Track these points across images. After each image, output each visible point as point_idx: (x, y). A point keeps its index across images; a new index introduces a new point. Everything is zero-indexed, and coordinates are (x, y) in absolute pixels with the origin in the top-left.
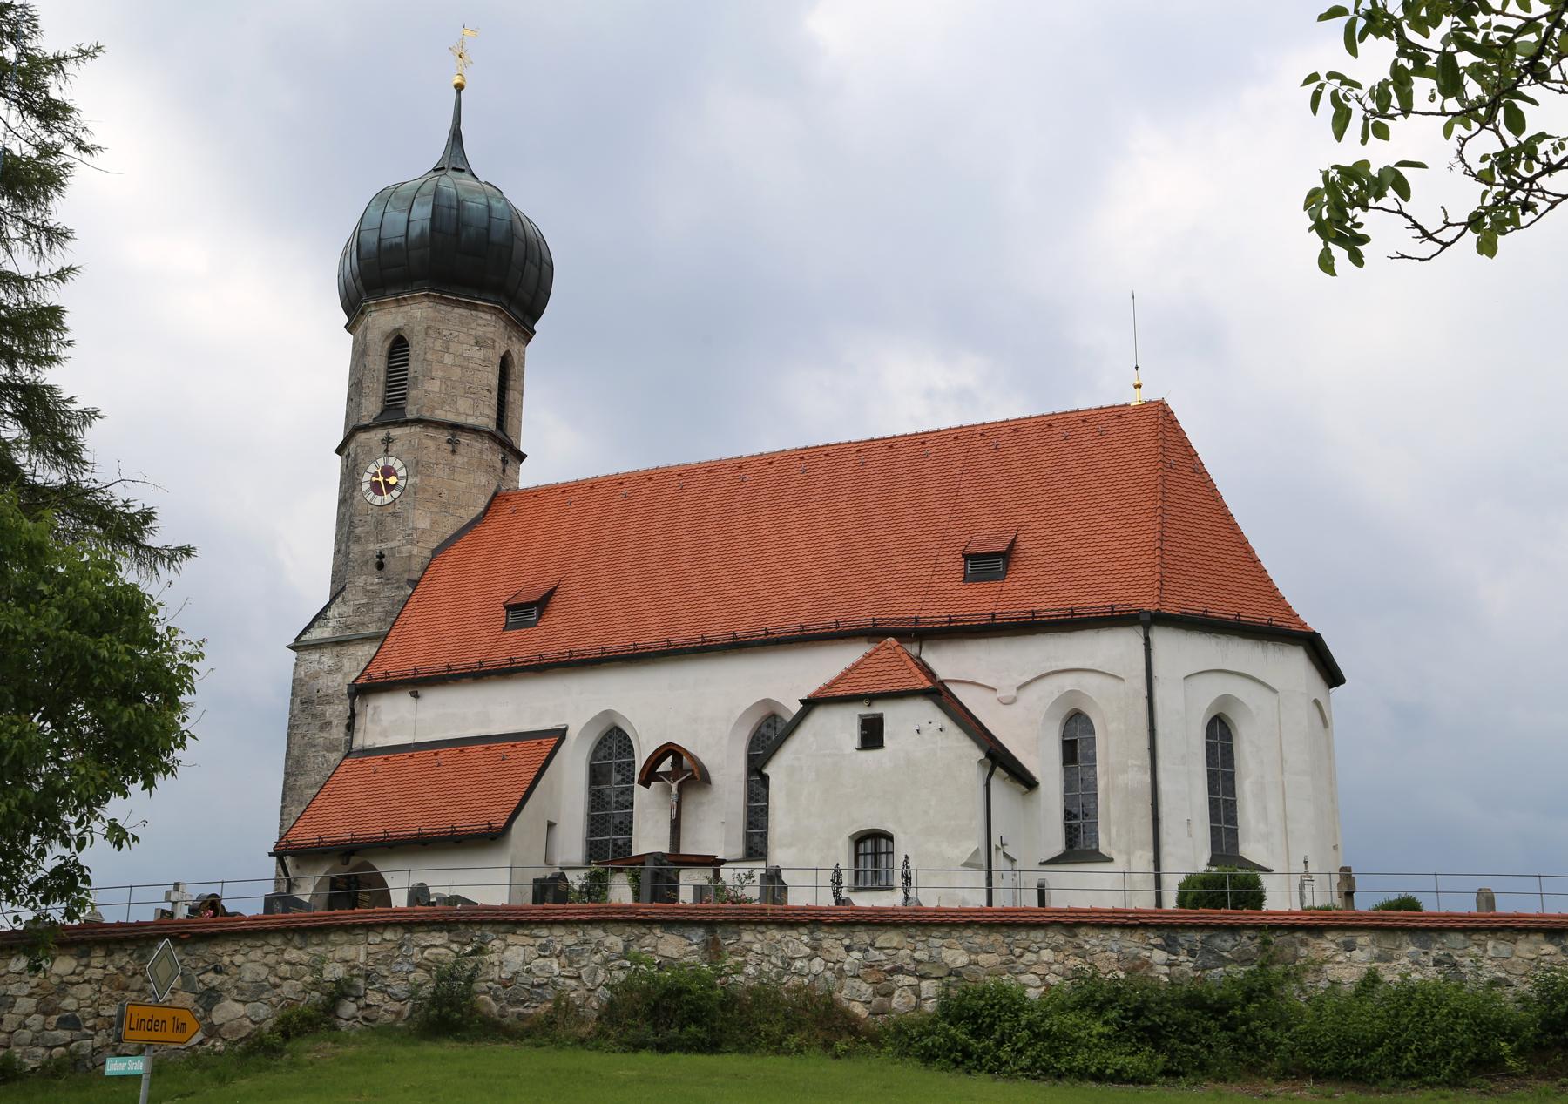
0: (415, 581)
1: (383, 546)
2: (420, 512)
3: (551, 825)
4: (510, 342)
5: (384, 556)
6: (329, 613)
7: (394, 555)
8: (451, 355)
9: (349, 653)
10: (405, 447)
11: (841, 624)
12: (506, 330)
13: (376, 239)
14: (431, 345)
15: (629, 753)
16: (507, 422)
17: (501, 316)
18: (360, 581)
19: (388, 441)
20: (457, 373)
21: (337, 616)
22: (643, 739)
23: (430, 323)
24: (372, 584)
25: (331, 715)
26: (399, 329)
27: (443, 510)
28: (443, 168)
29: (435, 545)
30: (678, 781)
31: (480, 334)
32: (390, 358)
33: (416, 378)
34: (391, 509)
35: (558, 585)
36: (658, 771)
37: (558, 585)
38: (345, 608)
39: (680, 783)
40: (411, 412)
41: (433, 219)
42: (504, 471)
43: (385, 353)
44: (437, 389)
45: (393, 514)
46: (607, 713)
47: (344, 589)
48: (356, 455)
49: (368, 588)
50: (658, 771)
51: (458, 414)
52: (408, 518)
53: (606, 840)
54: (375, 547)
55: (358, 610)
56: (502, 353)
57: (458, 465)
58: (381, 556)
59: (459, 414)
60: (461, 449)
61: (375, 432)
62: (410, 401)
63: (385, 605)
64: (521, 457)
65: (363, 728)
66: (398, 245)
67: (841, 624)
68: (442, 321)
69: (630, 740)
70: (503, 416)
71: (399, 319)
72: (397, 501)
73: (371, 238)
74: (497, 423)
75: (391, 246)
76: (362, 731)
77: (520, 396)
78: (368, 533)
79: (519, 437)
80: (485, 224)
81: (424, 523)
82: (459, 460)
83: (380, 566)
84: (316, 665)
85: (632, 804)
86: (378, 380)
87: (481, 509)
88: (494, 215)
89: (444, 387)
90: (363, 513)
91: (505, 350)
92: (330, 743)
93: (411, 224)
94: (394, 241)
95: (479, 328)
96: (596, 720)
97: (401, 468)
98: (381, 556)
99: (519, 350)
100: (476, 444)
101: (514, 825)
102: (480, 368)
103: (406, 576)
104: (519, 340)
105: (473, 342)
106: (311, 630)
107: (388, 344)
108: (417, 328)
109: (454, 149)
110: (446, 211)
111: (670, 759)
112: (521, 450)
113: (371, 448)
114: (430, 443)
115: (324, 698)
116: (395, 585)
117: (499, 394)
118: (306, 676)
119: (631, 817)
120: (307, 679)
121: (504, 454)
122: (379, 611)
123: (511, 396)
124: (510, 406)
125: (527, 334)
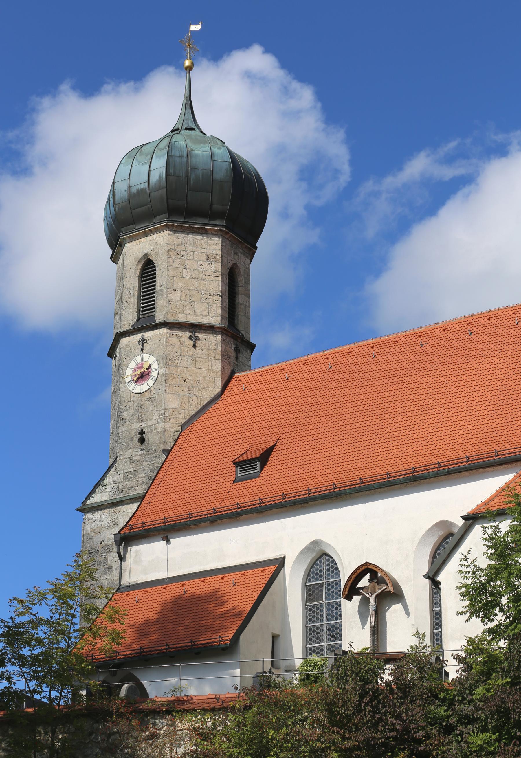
0: (168, 450)
2: (170, 395)
3: (275, 638)
4: (236, 257)
5: (144, 433)
6: (106, 481)
7: (152, 432)
9: (122, 511)
11: (499, 453)
12: (232, 247)
13: (126, 188)
14: (172, 264)
15: (336, 574)
16: (238, 320)
17: (227, 236)
18: (128, 454)
19: (143, 342)
20: (193, 284)
21: (112, 483)
22: (345, 562)
24: (136, 455)
25: (111, 561)
26: (146, 255)
27: (189, 392)
28: (178, 129)
29: (184, 421)
30: (375, 595)
31: (211, 251)
32: (141, 278)
33: (161, 291)
34: (147, 395)
35: (276, 443)
36: (358, 586)
37: (276, 443)
38: (118, 476)
39: (376, 596)
40: (159, 317)
42: (237, 358)
43: (138, 274)
44: (178, 298)
45: (150, 399)
46: (316, 543)
47: (115, 461)
48: (120, 355)
49: (134, 459)
50: (358, 586)
51: (196, 315)
52: (161, 401)
53: (322, 646)
54: (137, 426)
55: (127, 476)
56: (230, 265)
57: (199, 356)
58: (142, 432)
59: (197, 316)
60: (199, 343)
61: (133, 337)
62: (157, 309)
63: (147, 471)
64: (252, 347)
65: (128, 568)
66: (143, 190)
67: (499, 453)
69: (336, 564)
70: (234, 315)
71: (147, 246)
72: (152, 388)
73: (122, 189)
74: (229, 321)
75: (138, 191)
76: (128, 571)
77: (247, 298)
78: (131, 415)
79: (248, 331)
80: (209, 166)
81: (173, 404)
82: (199, 352)
83: (142, 441)
84: (98, 522)
85: (340, 615)
86: (134, 295)
87: (219, 389)
88: (216, 159)
89: (184, 295)
90: (128, 401)
91: (231, 263)
92: (113, 583)
93: (152, 173)
95: (209, 247)
96: (308, 549)
97: (154, 362)
98: (142, 432)
99: (244, 262)
100: (212, 338)
101: (242, 637)
102: (212, 278)
103: (162, 447)
104: (244, 255)
105: (205, 258)
106: (94, 495)
108: (160, 252)
110: (177, 159)
111: (368, 576)
112: (251, 341)
113: (131, 349)
114: (174, 340)
115: (106, 548)
116: (154, 455)
117: (229, 298)
118: (91, 531)
119: (340, 626)
120: (92, 534)
121: (236, 345)
122: (143, 477)
123: (240, 299)
125: (250, 249)
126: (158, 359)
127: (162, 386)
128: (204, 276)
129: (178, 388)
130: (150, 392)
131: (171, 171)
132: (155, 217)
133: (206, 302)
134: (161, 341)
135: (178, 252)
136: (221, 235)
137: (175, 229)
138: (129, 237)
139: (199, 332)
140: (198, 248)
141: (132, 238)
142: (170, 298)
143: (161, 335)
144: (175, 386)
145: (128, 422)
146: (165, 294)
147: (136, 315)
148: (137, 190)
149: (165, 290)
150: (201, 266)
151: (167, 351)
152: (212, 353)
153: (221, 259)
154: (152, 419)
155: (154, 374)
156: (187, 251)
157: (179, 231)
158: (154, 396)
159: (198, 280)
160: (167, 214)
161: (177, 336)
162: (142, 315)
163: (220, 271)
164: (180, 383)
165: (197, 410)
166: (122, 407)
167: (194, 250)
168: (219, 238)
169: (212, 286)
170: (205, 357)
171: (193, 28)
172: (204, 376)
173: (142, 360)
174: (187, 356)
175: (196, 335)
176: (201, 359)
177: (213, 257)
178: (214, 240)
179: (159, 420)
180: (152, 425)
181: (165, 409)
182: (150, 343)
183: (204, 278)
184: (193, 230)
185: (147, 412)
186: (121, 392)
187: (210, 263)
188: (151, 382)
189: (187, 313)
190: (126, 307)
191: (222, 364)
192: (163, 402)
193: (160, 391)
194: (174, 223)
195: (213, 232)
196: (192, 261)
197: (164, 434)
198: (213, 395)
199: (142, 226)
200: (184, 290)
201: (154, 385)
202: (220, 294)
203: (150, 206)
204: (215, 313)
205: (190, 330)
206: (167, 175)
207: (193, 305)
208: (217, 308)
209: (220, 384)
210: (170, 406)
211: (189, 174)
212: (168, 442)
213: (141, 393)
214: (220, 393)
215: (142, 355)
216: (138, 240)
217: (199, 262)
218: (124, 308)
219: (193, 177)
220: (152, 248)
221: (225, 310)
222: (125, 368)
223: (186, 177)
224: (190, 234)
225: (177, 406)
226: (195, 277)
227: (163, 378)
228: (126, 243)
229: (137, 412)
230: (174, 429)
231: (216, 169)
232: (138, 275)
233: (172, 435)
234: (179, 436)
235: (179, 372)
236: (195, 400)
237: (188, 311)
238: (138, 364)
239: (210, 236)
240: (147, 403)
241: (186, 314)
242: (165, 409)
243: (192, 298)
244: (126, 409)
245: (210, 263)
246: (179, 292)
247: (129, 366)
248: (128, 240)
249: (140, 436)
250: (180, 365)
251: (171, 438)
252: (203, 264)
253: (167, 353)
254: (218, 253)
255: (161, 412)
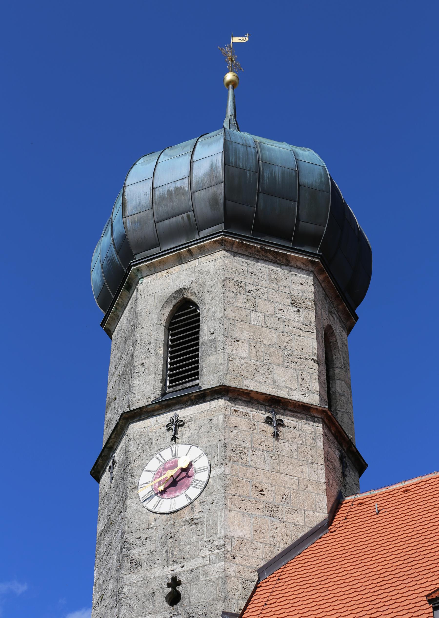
1: (177, 568)
2: (234, 513)
5: (179, 583)
7: (196, 580)
8: (261, 315)
10: (204, 429)
14: (232, 300)
23: (227, 275)
26: (181, 291)
29: (262, 563)
31: (296, 293)
34: (186, 515)
41: (226, 163)
43: (164, 322)
44: (244, 354)
45: (191, 522)
52: (215, 523)
68: (244, 273)
71: (182, 278)
72: (195, 503)
75: (170, 192)
78: (151, 553)
89: (253, 352)
90: (143, 527)
94: (173, 186)
95: (293, 286)
97: (200, 456)
100: (307, 426)
102: (301, 333)
105: (288, 301)
107: (167, 311)
109: (216, 162)
113: (151, 439)
124: (338, 398)
126: (208, 451)
127: (218, 497)
128: (287, 327)
129: (249, 503)
130: (192, 508)
131: (232, 160)
132: (198, 232)
133: (293, 368)
134: (215, 421)
135: (242, 285)
136: (312, 272)
137: (235, 249)
138: (148, 266)
139: (283, 414)
140: (275, 284)
141: (155, 268)
142: (229, 352)
143: (216, 410)
144: (242, 498)
145: (144, 565)
146: (220, 345)
147: (160, 385)
148: (168, 191)
149: (222, 338)
150: (281, 312)
151: (227, 436)
152: (308, 451)
153: (314, 306)
154: (197, 557)
155: (202, 477)
156: (256, 285)
157: (242, 254)
158: (199, 515)
159: (278, 331)
160: (223, 225)
161: (245, 415)
162: (169, 387)
163: (314, 324)
164: (252, 495)
165: (286, 546)
166: (131, 539)
167: (268, 286)
168: (309, 275)
169: (301, 344)
170: (296, 457)
171: (235, 40)
172: (296, 488)
173: (175, 455)
174: (262, 451)
175: (277, 418)
176: (289, 459)
177: (301, 302)
178: (302, 277)
179: (213, 557)
180: (197, 568)
181: (225, 537)
182: (191, 427)
183: (288, 331)
184: (266, 257)
185: (186, 545)
186: (129, 513)
187: (296, 309)
188: (193, 492)
189: (261, 380)
190: (141, 373)
191: (326, 473)
192: (220, 526)
193: (213, 506)
194: (235, 238)
195: (299, 264)
196: (266, 302)
197: (224, 583)
198: (314, 524)
199: (172, 246)
200: (253, 344)
201: (200, 497)
202: (317, 359)
203: (191, 213)
204: (310, 387)
205: (267, 408)
206: (225, 164)
207: (271, 369)
208: (313, 381)
209: (326, 507)
210: (234, 534)
211: (261, 169)
212: (232, 599)
213: (173, 513)
214: (326, 521)
215: (173, 447)
216: (165, 271)
217: (277, 305)
218: (137, 374)
219: (267, 174)
220: (192, 279)
221: (323, 388)
222: (138, 472)
223: (256, 172)
224: (261, 261)
225: (248, 536)
226: (272, 326)
227: (220, 483)
228: (142, 278)
229: (164, 547)
230: (243, 576)
231: (303, 172)
232: (164, 324)
233: (239, 586)
234: (256, 588)
235: (249, 476)
236: (281, 529)
237: (261, 377)
238: (167, 462)
239: (294, 269)
240: (186, 529)
241: (259, 382)
242: (225, 537)
243: (268, 358)
244: (139, 542)
245: (296, 309)
246: (246, 345)
247: (147, 468)
248: (145, 272)
249: (170, 589)
250: (252, 463)
251: (239, 593)
252: (285, 310)
253: (226, 441)
254: (308, 297)
255: (216, 543)
